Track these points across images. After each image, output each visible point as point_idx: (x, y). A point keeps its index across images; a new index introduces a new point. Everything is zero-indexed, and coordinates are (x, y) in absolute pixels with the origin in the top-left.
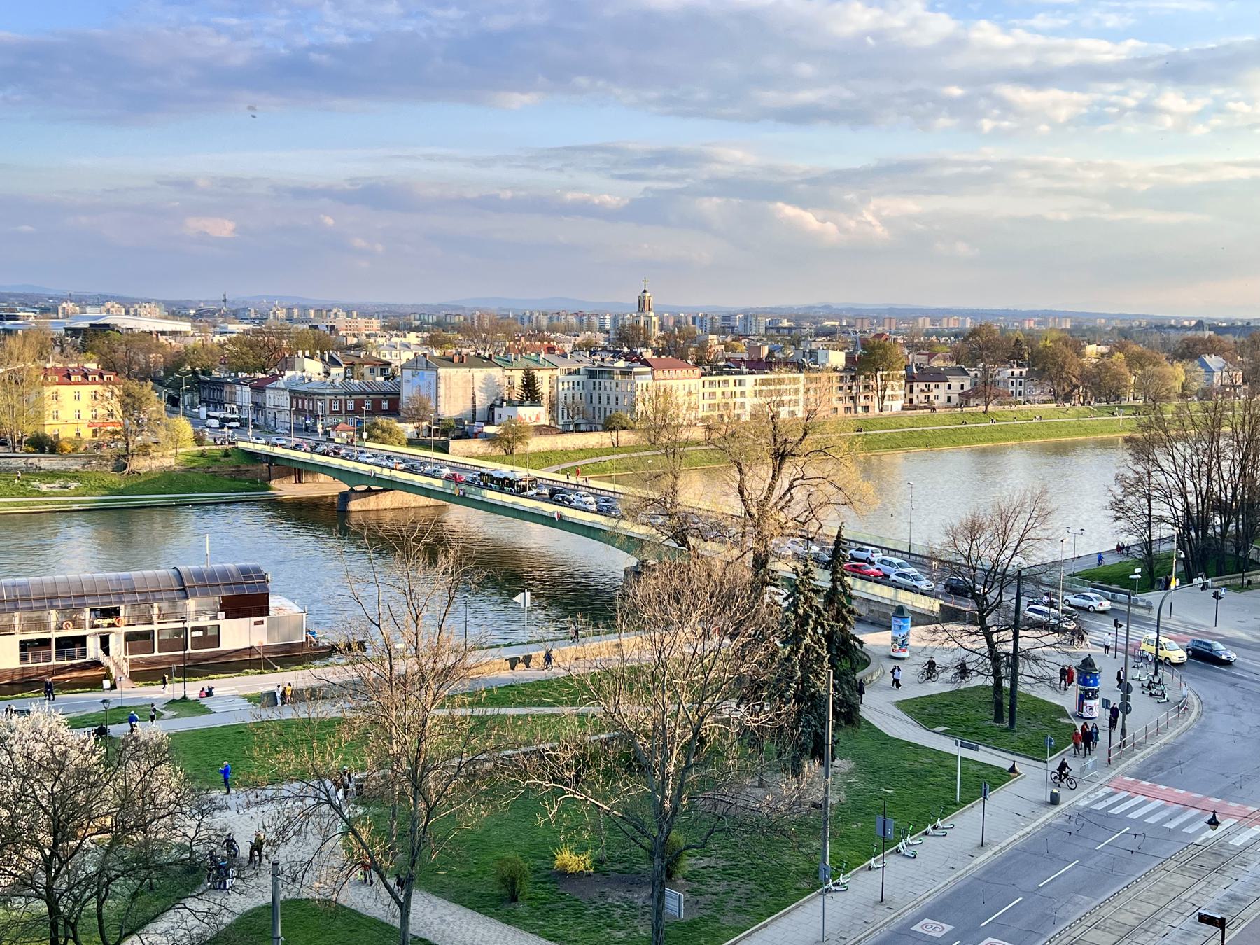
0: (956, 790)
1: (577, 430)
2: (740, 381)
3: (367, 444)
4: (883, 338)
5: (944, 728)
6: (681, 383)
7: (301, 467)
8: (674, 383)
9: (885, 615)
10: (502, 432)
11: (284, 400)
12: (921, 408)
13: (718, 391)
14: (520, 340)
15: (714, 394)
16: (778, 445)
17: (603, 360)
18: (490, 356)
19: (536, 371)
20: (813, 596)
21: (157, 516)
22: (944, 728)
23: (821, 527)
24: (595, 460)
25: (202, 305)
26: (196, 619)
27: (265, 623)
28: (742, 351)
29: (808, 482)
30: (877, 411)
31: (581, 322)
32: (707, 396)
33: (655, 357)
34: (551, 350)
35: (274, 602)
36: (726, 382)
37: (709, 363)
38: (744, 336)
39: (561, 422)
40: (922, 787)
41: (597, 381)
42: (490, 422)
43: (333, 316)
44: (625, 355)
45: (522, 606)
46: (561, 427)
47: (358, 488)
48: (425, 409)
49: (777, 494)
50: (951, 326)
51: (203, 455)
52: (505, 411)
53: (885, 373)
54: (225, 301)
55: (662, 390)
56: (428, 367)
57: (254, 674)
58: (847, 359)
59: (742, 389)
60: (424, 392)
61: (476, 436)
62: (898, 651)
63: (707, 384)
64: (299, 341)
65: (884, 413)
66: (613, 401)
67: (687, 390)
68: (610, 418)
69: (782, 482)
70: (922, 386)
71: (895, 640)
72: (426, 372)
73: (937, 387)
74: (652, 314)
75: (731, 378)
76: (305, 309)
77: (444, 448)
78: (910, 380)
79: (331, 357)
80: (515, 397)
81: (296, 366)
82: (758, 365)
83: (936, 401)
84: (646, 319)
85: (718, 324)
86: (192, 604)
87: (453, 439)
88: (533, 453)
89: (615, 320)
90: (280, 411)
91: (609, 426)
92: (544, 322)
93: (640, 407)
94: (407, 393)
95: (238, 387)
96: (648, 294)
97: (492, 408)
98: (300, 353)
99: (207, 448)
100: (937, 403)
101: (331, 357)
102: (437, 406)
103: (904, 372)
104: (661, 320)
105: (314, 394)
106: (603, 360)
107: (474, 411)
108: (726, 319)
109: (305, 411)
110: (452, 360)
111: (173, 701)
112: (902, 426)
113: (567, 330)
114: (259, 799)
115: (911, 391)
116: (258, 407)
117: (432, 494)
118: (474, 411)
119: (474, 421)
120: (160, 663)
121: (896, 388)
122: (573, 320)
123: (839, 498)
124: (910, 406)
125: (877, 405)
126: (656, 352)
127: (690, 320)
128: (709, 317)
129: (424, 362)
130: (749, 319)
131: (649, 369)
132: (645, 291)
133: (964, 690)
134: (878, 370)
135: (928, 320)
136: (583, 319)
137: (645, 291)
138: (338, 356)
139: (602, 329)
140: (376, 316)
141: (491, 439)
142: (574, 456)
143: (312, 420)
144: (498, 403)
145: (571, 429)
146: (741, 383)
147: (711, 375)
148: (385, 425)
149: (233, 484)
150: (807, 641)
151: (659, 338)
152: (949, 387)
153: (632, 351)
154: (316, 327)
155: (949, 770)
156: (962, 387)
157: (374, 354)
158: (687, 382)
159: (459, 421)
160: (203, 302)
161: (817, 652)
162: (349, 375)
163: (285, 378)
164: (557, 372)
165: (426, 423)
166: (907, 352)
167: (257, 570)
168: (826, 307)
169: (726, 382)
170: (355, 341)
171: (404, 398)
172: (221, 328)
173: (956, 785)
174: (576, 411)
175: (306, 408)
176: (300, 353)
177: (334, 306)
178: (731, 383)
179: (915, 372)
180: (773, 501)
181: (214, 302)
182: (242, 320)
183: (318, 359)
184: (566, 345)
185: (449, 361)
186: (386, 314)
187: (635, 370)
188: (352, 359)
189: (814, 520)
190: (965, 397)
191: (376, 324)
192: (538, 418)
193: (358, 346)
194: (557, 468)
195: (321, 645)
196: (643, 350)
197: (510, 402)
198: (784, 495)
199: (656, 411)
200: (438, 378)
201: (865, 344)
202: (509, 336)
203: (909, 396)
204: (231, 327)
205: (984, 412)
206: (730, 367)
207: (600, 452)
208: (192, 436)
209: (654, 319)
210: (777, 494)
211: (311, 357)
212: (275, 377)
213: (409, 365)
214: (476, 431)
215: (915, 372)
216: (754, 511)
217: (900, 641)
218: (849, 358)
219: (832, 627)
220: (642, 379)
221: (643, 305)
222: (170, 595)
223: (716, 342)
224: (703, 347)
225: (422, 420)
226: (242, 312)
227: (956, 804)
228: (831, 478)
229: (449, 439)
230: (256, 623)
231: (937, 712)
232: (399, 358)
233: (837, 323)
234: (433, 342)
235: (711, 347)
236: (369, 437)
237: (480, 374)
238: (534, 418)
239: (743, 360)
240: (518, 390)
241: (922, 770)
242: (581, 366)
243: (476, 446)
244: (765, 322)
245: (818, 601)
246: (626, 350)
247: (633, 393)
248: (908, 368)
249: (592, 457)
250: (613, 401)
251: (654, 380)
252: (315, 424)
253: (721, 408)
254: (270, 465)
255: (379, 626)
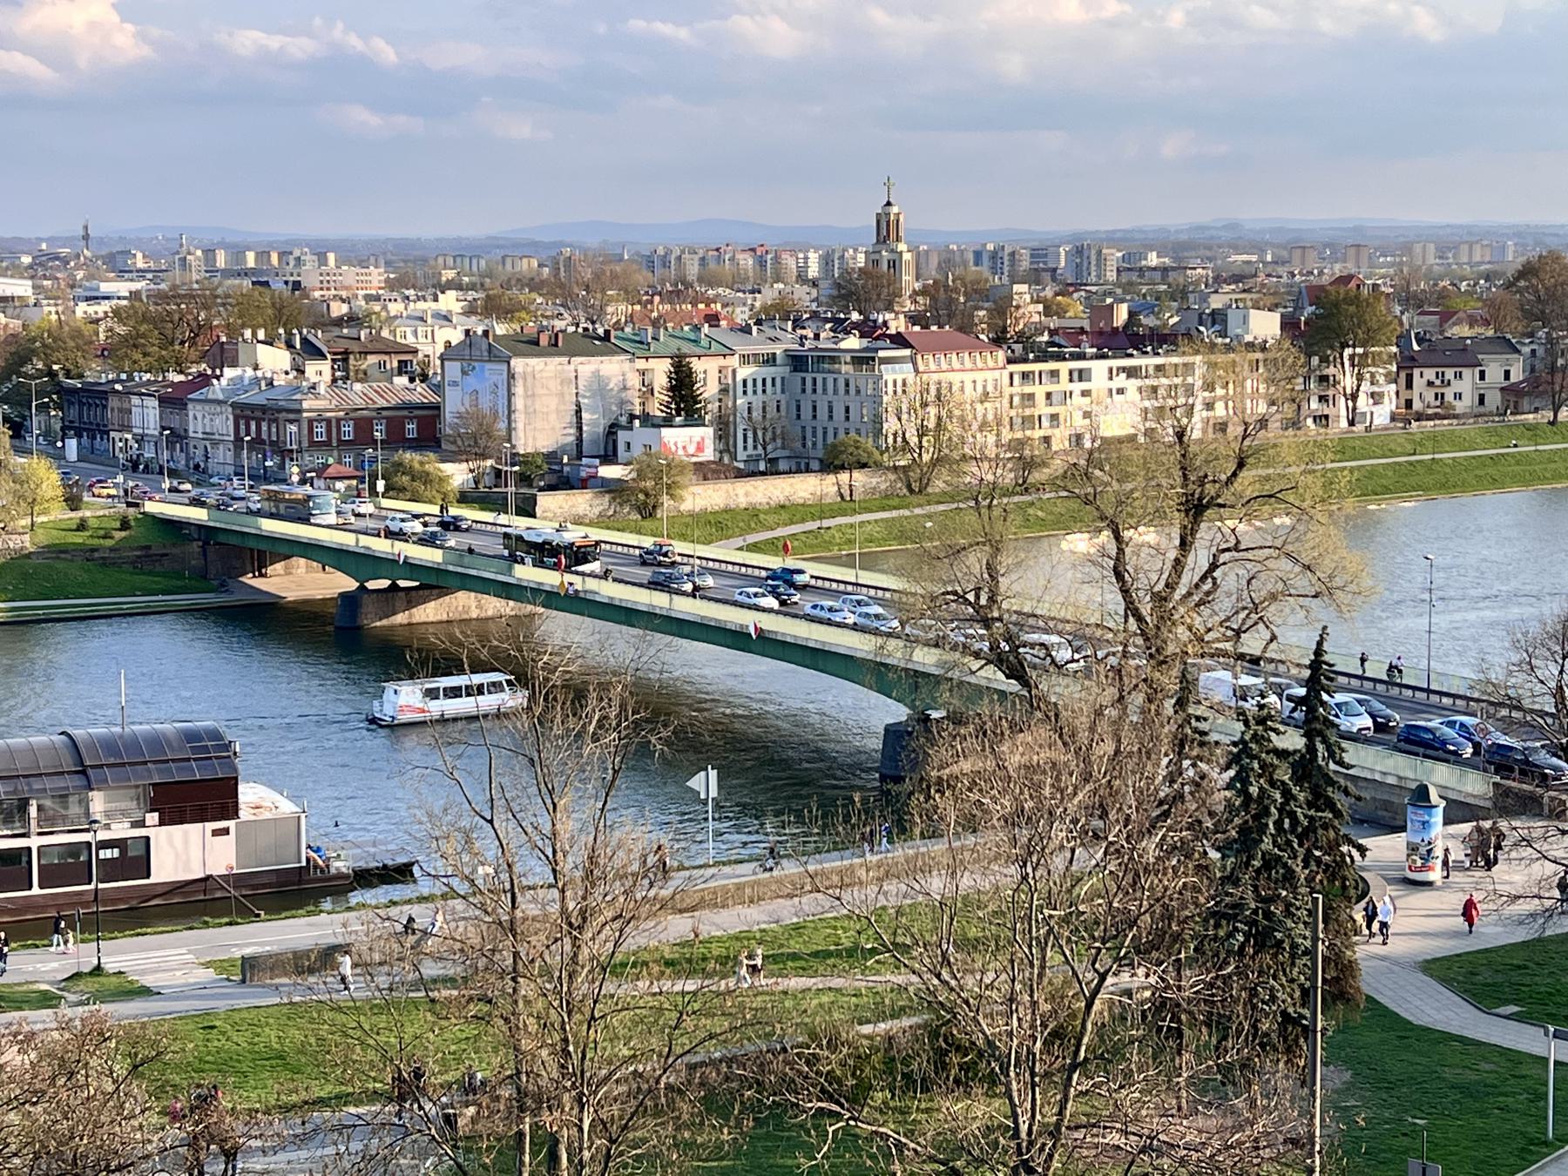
0: (1546, 1118)
1: (773, 470)
2: (1081, 371)
3: (386, 503)
4: (1353, 284)
5: (1514, 1009)
6: (968, 377)
7: (262, 546)
8: (955, 378)
9: (1387, 805)
10: (634, 475)
11: (224, 424)
12: (1430, 418)
13: (1039, 391)
14: (652, 302)
15: (1031, 396)
16: (1191, 486)
17: (817, 337)
18: (607, 332)
19: (694, 360)
20: (1276, 762)
21: (66, 632)
22: (1514, 1009)
23: (1273, 638)
24: (812, 525)
25: (44, 246)
26: (107, 827)
27: (233, 831)
28: (1076, 312)
29: (1249, 555)
30: (1344, 424)
31: (761, 263)
32: (1016, 400)
33: (917, 328)
34: (713, 319)
35: (248, 793)
36: (1054, 374)
37: (1021, 337)
38: (1077, 286)
39: (741, 455)
40: (1482, 1114)
41: (809, 377)
42: (609, 457)
43: (292, 263)
44: (856, 325)
45: (703, 796)
46: (741, 466)
47: (372, 585)
48: (489, 434)
49: (1188, 579)
50: (1477, 258)
51: (82, 526)
52: (638, 436)
53: (1359, 350)
54: (86, 237)
55: (933, 391)
56: (493, 355)
57: (220, 925)
58: (1284, 326)
59: (1084, 386)
60: (485, 403)
61: (583, 484)
62: (1420, 870)
63: (1016, 378)
64: (246, 312)
65: (1359, 428)
66: (839, 413)
67: (980, 389)
68: (834, 446)
69: (1199, 559)
70: (1430, 374)
71: (1413, 849)
72: (488, 366)
73: (1459, 376)
74: (902, 247)
75: (1064, 367)
76: (238, 253)
77: (527, 509)
78: (1408, 363)
79: (305, 341)
80: (655, 410)
81: (242, 358)
82: (1127, 340)
83: (1457, 403)
84: (892, 256)
85: (1025, 264)
86: (98, 803)
87: (541, 489)
88: (692, 515)
89: (826, 261)
90: (215, 443)
91: (831, 465)
92: (693, 270)
93: (891, 425)
94: (454, 404)
95: (135, 400)
96: (895, 210)
97: (612, 429)
98: (248, 333)
99: (88, 514)
100: (1460, 407)
101: (305, 341)
102: (510, 429)
103: (1394, 349)
104: (919, 257)
105: (280, 411)
106: (817, 337)
107: (580, 439)
108: (1037, 254)
109: (263, 442)
110: (536, 343)
111: (77, 976)
112: (1394, 454)
113: (737, 282)
114: (309, 1127)
115: (1409, 385)
116: (177, 437)
117: (514, 592)
118: (580, 439)
119: (580, 456)
120: (44, 908)
121: (1382, 380)
122: (747, 261)
123: (1303, 583)
124: (1407, 414)
125: (1343, 412)
126: (913, 319)
127: (971, 257)
128: (1008, 250)
129: (485, 347)
130: (1086, 254)
131: (907, 352)
132: (889, 204)
133: (1551, 939)
134: (1344, 346)
135: (1431, 248)
136: (767, 265)
137: (889, 204)
138: (318, 338)
139: (802, 278)
140: (372, 259)
141: (614, 489)
142: (771, 519)
143: (277, 459)
144: (623, 420)
145: (762, 467)
146: (1083, 375)
147: (1025, 361)
148: (417, 466)
149: (140, 579)
150: (1267, 844)
151: (915, 293)
152: (1482, 376)
153: (867, 319)
154: (266, 284)
155: (1530, 1083)
156: (1507, 375)
157: (385, 333)
158: (979, 377)
159: (552, 457)
160: (48, 240)
161: (1285, 865)
162: (338, 374)
163: (224, 381)
164: (734, 361)
165: (489, 462)
166: (1397, 309)
167: (215, 735)
168: (1232, 226)
169: (1054, 374)
170: (344, 309)
171: (449, 415)
172: (86, 289)
173: (1546, 1109)
174: (769, 435)
175: (264, 436)
176: (248, 333)
177: (299, 243)
178: (1064, 376)
179: (1416, 347)
180: (1181, 590)
181: (66, 242)
182: (122, 273)
183: (283, 345)
184: (738, 310)
185: (531, 345)
186: (389, 257)
187: (881, 354)
188: (342, 345)
189: (1261, 626)
190: (1514, 396)
191: (376, 277)
192: (700, 448)
193: (352, 319)
194: (740, 542)
195: (333, 871)
196: (889, 316)
197: (647, 419)
198: (1203, 578)
199: (922, 432)
200: (511, 376)
201: (1317, 294)
202: (630, 296)
203: (1405, 395)
204: (105, 288)
205: (1552, 423)
206: (1060, 346)
207: (819, 510)
208: (60, 492)
209: (907, 256)
210: (1188, 579)
211: (269, 342)
212: (204, 380)
213: (450, 353)
214: (583, 474)
215: (1416, 347)
216: (1145, 609)
217: (1423, 850)
218: (1288, 324)
219: (1311, 819)
220: (894, 371)
221: (886, 229)
222: (60, 782)
223: (1027, 298)
224: (1002, 307)
225: (484, 457)
226: (119, 258)
227: (1546, 1143)
228: (1289, 548)
229: (534, 491)
230: (216, 833)
231: (1500, 978)
232: (432, 343)
233: (1254, 258)
234: (492, 307)
235: (1018, 307)
236: (388, 488)
237: (587, 366)
238: (691, 450)
239: (1082, 331)
240: (661, 396)
241: (1478, 1083)
242: (778, 349)
243: (581, 502)
244: (1114, 256)
245: (1284, 774)
246: (855, 316)
247: (877, 399)
248: (1403, 340)
249: (803, 521)
250: (839, 413)
251: (917, 371)
252: (282, 466)
253: (1045, 423)
254: (206, 543)
255: (491, 822)
